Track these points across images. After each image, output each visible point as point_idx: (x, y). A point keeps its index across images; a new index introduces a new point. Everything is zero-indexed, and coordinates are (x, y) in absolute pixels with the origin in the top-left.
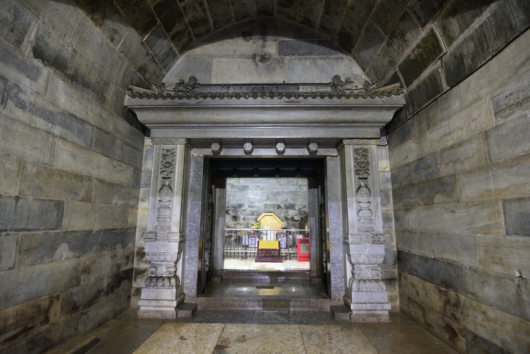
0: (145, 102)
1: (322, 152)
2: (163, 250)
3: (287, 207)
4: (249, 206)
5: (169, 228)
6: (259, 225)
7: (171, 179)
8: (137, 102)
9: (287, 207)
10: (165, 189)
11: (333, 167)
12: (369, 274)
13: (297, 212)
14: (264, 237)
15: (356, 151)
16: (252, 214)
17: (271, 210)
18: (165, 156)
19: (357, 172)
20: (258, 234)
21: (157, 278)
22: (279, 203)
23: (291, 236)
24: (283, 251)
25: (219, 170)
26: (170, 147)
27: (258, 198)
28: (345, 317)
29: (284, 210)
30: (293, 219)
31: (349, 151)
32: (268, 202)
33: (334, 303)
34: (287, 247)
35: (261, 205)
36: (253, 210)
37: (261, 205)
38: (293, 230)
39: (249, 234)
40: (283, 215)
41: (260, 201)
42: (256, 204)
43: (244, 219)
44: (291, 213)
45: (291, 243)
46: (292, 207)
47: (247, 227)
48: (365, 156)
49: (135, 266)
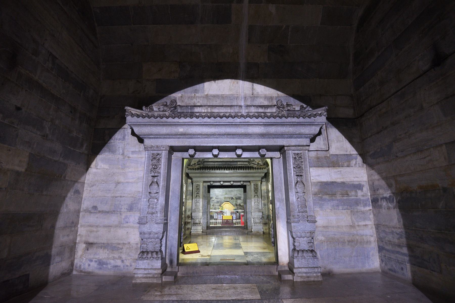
0: (192, 171)
1: (245, 184)
2: (198, 215)
3: (237, 199)
4: (216, 198)
5: (199, 208)
6: (222, 208)
7: (158, 178)
8: (190, 171)
9: (237, 199)
10: (198, 197)
11: (248, 188)
12: (257, 221)
13: (242, 201)
14: (225, 214)
15: (254, 185)
16: (218, 202)
17: (228, 200)
18: (197, 186)
19: (254, 191)
20: (222, 213)
21: (196, 224)
22: (232, 196)
23: (238, 214)
24: (234, 221)
25: (210, 187)
26: (198, 183)
27: (221, 193)
28: (251, 233)
29: (235, 200)
30: (240, 205)
31: (252, 184)
32: (226, 196)
33: (248, 231)
34: (236, 219)
35: (222, 198)
36: (218, 200)
37: (222, 198)
38: (240, 211)
39: (217, 213)
40: (234, 203)
41: (222, 195)
42: (220, 197)
43: (213, 205)
44: (239, 202)
45: (238, 217)
46: (239, 198)
47: (215, 209)
48: (257, 186)
49: (187, 221)
